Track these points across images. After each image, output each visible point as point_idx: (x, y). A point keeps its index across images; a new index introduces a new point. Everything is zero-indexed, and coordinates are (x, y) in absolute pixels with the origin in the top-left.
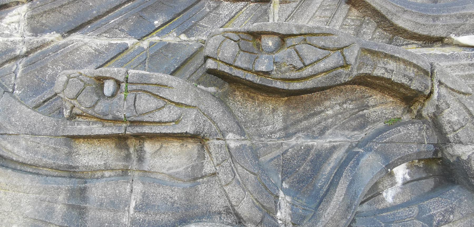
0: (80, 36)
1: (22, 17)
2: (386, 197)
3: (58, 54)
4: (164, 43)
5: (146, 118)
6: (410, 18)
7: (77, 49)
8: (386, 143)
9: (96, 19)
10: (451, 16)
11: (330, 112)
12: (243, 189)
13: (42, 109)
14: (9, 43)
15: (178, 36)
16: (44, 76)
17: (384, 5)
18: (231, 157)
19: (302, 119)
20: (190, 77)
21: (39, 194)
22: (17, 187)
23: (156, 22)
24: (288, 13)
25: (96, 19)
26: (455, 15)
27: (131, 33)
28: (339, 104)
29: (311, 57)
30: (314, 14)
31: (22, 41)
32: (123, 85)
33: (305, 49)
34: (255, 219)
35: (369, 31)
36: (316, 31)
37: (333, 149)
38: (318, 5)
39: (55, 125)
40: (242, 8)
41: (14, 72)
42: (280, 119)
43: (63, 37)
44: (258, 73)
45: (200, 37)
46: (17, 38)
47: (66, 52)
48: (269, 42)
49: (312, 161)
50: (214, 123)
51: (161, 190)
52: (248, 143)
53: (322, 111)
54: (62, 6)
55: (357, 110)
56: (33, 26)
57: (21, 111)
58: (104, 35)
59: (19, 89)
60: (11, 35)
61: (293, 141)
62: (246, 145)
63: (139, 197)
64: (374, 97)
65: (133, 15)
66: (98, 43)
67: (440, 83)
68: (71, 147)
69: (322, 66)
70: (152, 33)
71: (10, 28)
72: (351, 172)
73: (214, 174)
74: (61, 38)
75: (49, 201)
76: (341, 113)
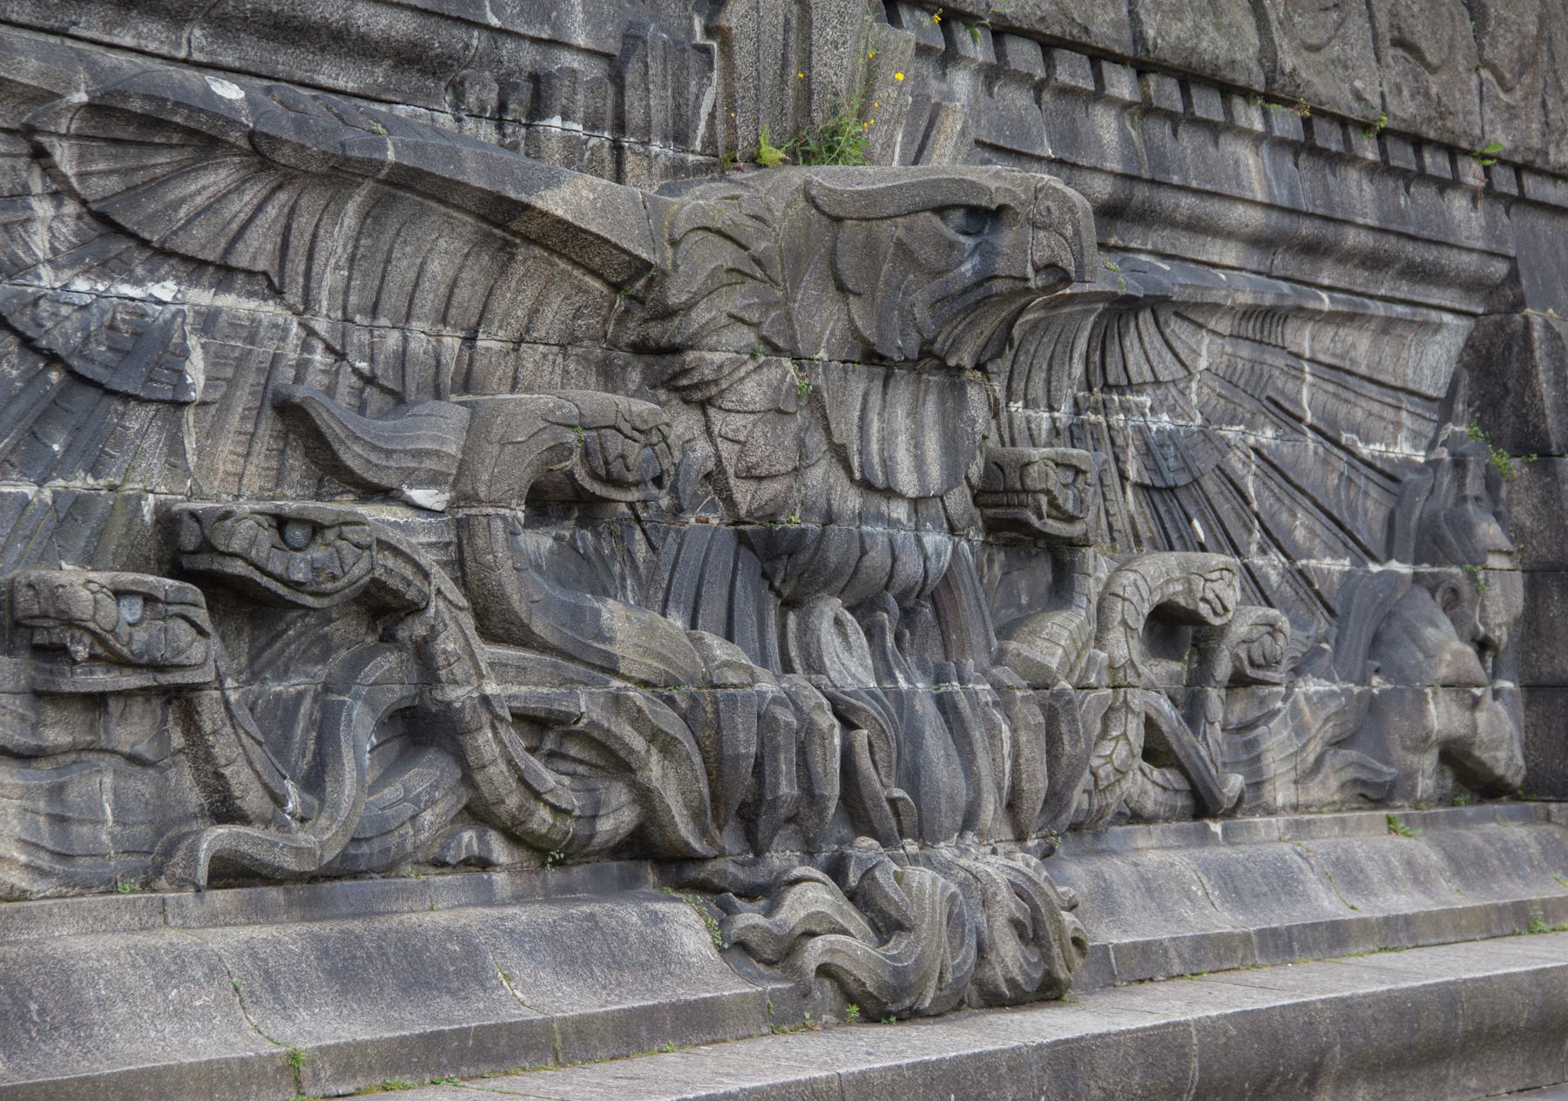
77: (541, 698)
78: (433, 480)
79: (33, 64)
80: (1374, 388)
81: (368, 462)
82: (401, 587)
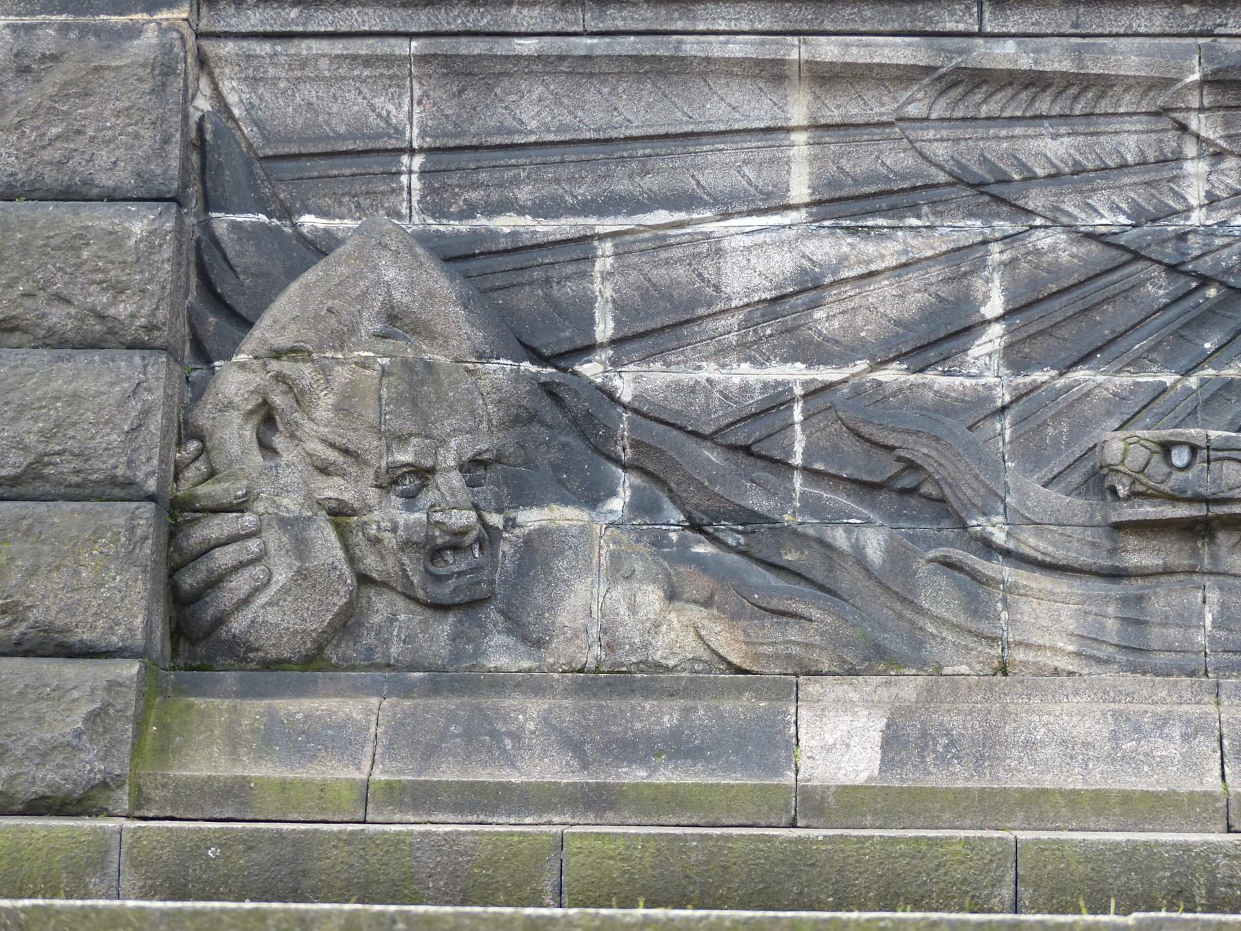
0: (1087, 372)
7: (1087, 394)
14: (980, 389)
16: (1043, 439)
22: (1054, 594)
23: (1207, 345)
27: (1167, 365)
39: (1087, 511)
43: (1061, 375)
46: (990, 379)
47: (1071, 400)
57: (1036, 493)
58: (1126, 369)
60: (980, 375)
63: (1216, 608)
65: (1170, 335)
75: (1096, 614)
79: (1134, 59)
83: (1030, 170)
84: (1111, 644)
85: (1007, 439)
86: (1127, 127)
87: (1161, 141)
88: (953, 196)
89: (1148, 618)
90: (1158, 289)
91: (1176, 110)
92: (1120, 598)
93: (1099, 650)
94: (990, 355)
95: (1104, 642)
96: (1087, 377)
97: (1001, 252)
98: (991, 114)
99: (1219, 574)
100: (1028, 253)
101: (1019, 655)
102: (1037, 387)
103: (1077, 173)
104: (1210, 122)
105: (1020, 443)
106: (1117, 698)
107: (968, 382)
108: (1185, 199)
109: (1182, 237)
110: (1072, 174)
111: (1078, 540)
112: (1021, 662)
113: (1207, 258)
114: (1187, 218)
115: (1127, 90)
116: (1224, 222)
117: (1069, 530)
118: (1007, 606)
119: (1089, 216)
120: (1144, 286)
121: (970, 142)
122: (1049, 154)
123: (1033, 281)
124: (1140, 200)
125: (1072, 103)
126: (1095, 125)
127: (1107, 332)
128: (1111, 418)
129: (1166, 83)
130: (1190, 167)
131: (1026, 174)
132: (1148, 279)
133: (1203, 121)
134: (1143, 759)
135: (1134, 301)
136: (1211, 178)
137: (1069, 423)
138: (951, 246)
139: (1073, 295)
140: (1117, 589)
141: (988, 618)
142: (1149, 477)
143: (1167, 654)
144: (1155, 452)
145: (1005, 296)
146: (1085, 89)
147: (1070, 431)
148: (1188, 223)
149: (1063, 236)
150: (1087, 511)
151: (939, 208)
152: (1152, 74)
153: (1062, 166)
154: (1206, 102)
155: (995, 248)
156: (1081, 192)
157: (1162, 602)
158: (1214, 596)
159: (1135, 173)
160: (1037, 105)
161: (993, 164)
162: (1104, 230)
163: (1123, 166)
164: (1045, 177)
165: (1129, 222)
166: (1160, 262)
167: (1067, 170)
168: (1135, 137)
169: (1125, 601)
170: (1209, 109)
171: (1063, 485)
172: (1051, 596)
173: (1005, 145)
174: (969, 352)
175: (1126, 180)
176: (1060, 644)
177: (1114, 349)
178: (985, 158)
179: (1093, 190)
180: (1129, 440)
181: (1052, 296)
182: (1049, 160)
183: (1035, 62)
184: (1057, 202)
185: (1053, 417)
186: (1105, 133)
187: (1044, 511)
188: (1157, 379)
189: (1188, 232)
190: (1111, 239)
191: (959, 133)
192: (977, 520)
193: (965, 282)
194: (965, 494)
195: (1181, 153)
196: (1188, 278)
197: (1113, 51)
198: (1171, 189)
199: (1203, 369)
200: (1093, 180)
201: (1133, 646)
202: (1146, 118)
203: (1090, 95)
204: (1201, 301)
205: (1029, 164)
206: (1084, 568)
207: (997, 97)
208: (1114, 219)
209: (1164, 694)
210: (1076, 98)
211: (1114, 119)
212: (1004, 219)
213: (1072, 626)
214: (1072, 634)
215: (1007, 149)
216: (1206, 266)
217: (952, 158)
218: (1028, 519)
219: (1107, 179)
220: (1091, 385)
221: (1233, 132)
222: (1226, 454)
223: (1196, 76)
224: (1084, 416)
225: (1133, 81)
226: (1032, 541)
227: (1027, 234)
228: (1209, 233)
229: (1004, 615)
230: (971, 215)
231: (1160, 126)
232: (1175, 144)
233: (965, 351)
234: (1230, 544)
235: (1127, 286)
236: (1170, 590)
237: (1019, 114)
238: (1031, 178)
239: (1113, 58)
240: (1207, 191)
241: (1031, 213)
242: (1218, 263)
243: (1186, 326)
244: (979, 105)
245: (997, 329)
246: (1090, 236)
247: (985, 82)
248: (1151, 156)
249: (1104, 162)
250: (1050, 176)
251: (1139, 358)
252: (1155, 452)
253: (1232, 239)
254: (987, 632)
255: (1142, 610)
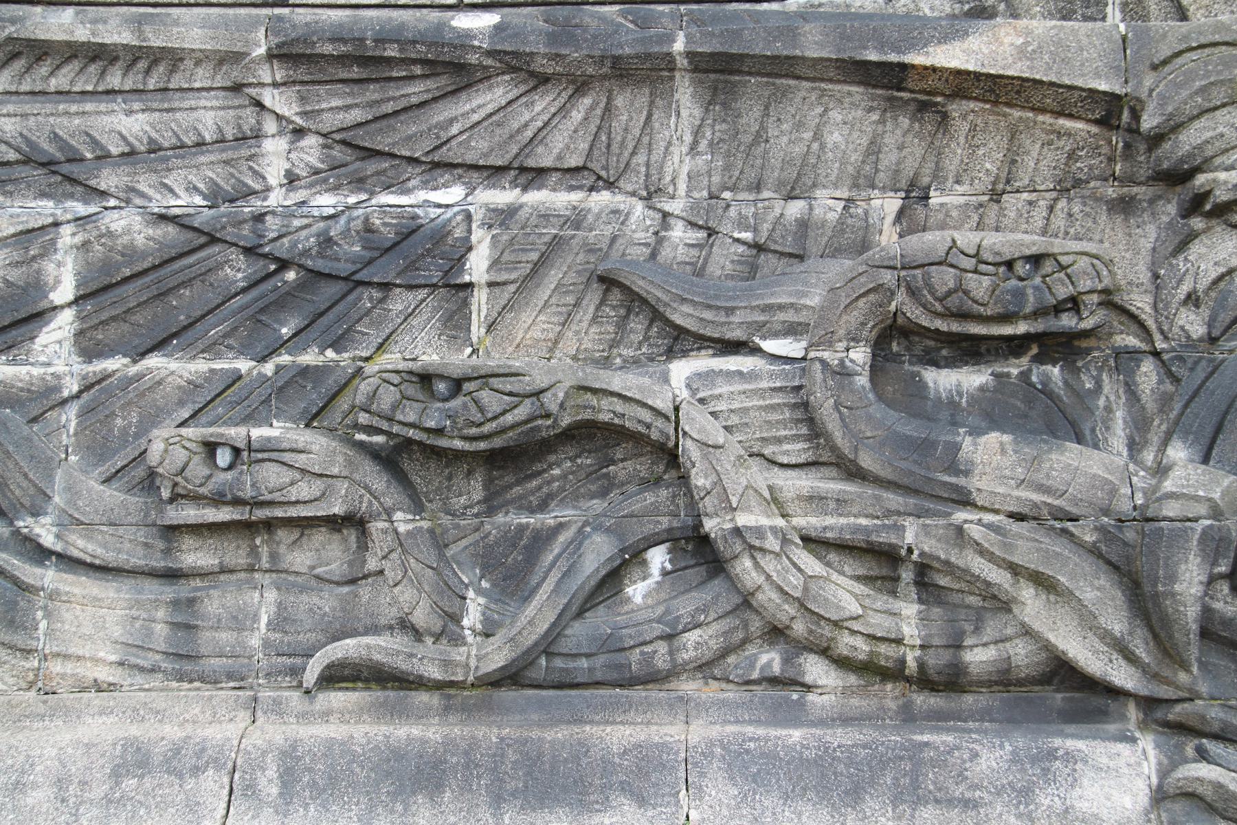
0: (160, 359)
1: (67, 334)
2: (634, 596)
3: (129, 392)
4: (299, 366)
5: (277, 496)
6: (691, 312)
7: (159, 383)
8: (623, 517)
9: (186, 328)
10: (753, 308)
11: (556, 472)
12: (418, 590)
13: (115, 484)
14: (49, 378)
15: (322, 353)
16: (111, 430)
17: (652, 290)
18: (401, 545)
19: (512, 483)
20: (343, 420)
21: (130, 609)
22: (99, 600)
23: (284, 330)
24: (503, 302)
25: (186, 328)
26: (758, 306)
27: (242, 352)
28: (570, 459)
29: (494, 408)
30: (546, 302)
31: (70, 371)
32: (245, 454)
33: (485, 396)
34: (433, 629)
35: (640, 327)
36: (502, 371)
37: (560, 527)
38: (553, 286)
39: (142, 510)
40: (426, 298)
41: (64, 427)
42: (479, 486)
43: (135, 362)
44: (428, 430)
45: (357, 352)
46: (60, 368)
47: (141, 389)
48: (441, 387)
49: (525, 547)
50: (375, 498)
51: (304, 597)
52: (425, 524)
53: (544, 471)
54: (129, 309)
55: (596, 467)
56: (82, 346)
57: (89, 491)
58: (201, 356)
59: (75, 453)
60: (49, 364)
61: (500, 518)
62: (421, 528)
63: (273, 609)
64: (624, 445)
65: (247, 320)
66: (193, 370)
67: (685, 433)
68: (169, 541)
69: (509, 418)
70: (278, 349)
71: (47, 352)
72: (568, 560)
73: (381, 572)
74: (131, 365)
75: (144, 619)
76: (573, 473)
77: (857, 529)
78: (792, 330)
79: (197, 32)
80: (414, 100)
81: (702, 319)
82: (640, 428)
83: (103, 148)
84: (157, 652)
85: (72, 431)
86: (203, 103)
87: (240, 118)
88: (23, 175)
89: (199, 623)
90: (237, 271)
91: (250, 85)
92: (171, 602)
93: (145, 658)
94: (60, 342)
95: (150, 649)
96: (160, 365)
97: (74, 234)
98: (60, 89)
99: (278, 571)
100: (101, 236)
101: (56, 667)
102: (109, 376)
103: (154, 151)
104: (284, 98)
105: (86, 436)
106: (147, 717)
107: (36, 371)
108: (264, 178)
109: (259, 218)
110: (150, 152)
111: (130, 541)
112: (57, 674)
113: (285, 240)
114: (265, 199)
115: (198, 63)
116: (303, 202)
117: (121, 530)
118: (48, 615)
119: (164, 196)
120: (222, 269)
121: (40, 118)
122: (124, 132)
123: (107, 266)
124: (219, 180)
125: (145, 78)
126: (170, 100)
127: (182, 317)
128: (183, 407)
129: (234, 57)
130: (269, 145)
131: (99, 153)
132: (225, 262)
133: (277, 97)
134: (142, 799)
135: (211, 285)
136: (291, 156)
137: (140, 413)
138: (20, 228)
139: (147, 279)
140: (169, 592)
141: (25, 628)
142: (186, 480)
143: (217, 659)
144: (195, 453)
145: (76, 280)
146: (155, 62)
147: (140, 422)
148: (265, 204)
149: (138, 218)
150: (142, 510)
151: (8, 188)
152: (218, 47)
153: (136, 143)
154: (278, 78)
155: (66, 230)
156: (155, 171)
157: (216, 603)
158: (271, 595)
159: (211, 152)
160: (108, 78)
161: (65, 141)
162: (177, 211)
163: (200, 144)
164: (119, 156)
165: (205, 203)
166: (236, 245)
167: (142, 148)
168: (212, 113)
169: (176, 604)
170: (284, 84)
171: (126, 479)
172: (96, 601)
173: (77, 122)
174: (37, 340)
175: (202, 159)
176: (102, 654)
177: (190, 334)
178: (55, 133)
179: (169, 170)
180: (171, 441)
181: (126, 280)
182: (124, 138)
183: (93, 34)
184: (131, 182)
185: (123, 408)
186: (180, 109)
187: (96, 511)
188: (232, 366)
189: (266, 214)
190: (186, 221)
191: (27, 108)
192: (24, 521)
193: (36, 266)
194: (13, 493)
195: (259, 130)
196: (267, 261)
197: (176, 23)
198: (250, 168)
199: (280, 355)
200: (168, 159)
201: (181, 652)
202: (223, 93)
203: (161, 69)
204: (279, 284)
205: (103, 141)
206: (136, 570)
207: (64, 70)
208: (190, 200)
209: (197, 711)
210: (148, 72)
211: (190, 95)
212: (78, 200)
213: (117, 632)
214: (116, 642)
215: (79, 126)
216: (283, 248)
217: (21, 134)
218: (77, 520)
219: (183, 157)
220: (164, 373)
221: (309, 108)
222: (266, 455)
223: (261, 50)
224: (155, 405)
225: (200, 55)
226: (81, 543)
227: (100, 216)
228: (288, 212)
229: (43, 625)
230: (43, 195)
231: (236, 102)
232: (254, 121)
233: (32, 339)
234: (290, 541)
235: (203, 270)
236: (225, 592)
237: (90, 88)
238: (103, 157)
239: (175, 30)
240: (287, 171)
241: (104, 194)
242: (294, 245)
243: (262, 310)
244: (46, 79)
245: (67, 316)
246: (163, 218)
247: (46, 54)
248: (230, 133)
249: (180, 140)
250: (123, 155)
251: (215, 344)
252: (195, 453)
253: (311, 219)
254: (21, 644)
255: (194, 614)
